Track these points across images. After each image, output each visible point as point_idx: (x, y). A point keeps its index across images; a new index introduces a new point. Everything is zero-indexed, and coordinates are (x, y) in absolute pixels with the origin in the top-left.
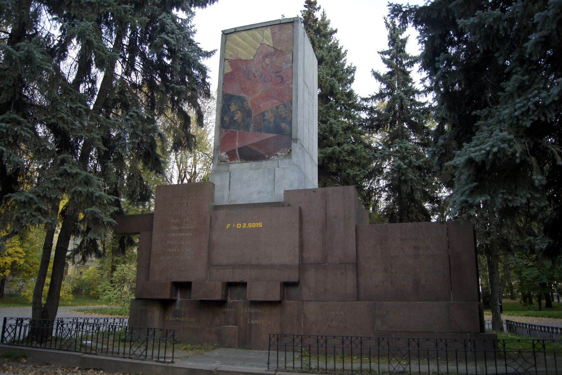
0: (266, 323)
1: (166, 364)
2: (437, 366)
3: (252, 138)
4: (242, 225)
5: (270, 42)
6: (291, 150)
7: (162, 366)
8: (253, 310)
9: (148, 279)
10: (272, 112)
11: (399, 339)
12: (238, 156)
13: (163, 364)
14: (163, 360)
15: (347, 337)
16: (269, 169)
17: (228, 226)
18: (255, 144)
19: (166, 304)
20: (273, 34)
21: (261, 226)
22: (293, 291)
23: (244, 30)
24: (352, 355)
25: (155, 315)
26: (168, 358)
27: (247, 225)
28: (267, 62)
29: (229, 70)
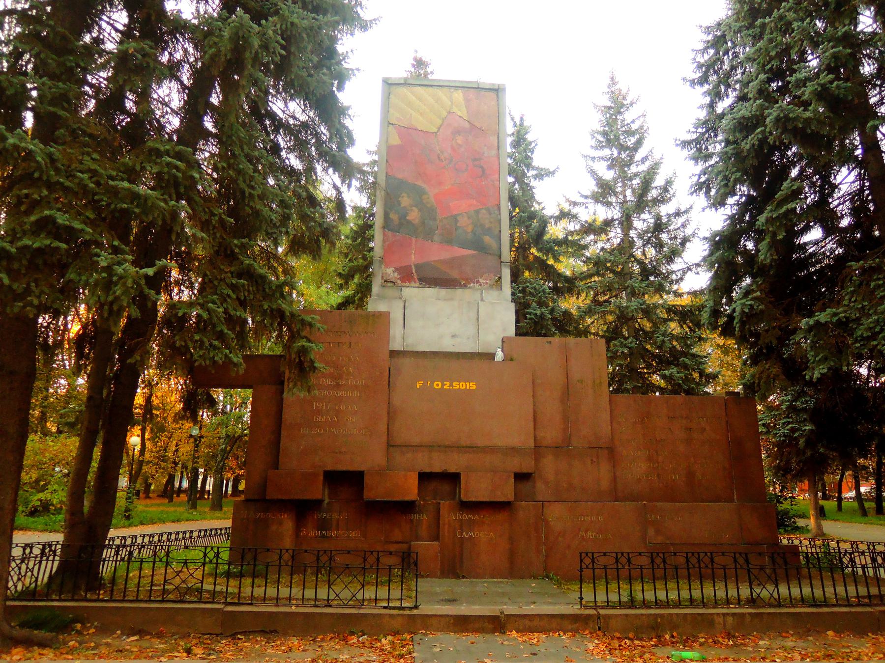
0: (486, 535)
1: (408, 612)
2: (866, 589)
3: (437, 253)
4: (443, 385)
5: (462, 112)
6: (500, 278)
7: (402, 615)
8: (465, 517)
9: (276, 465)
10: (469, 218)
11: (675, 554)
12: (416, 277)
13: (401, 612)
14: (398, 604)
15: (587, 554)
16: (469, 302)
17: (419, 384)
18: (444, 262)
19: (303, 509)
20: (467, 101)
21: (475, 387)
22: (525, 487)
23: (420, 85)
24: (665, 579)
25: (285, 527)
26: (382, 600)
27: (451, 385)
28: (459, 142)
29: (395, 141)
